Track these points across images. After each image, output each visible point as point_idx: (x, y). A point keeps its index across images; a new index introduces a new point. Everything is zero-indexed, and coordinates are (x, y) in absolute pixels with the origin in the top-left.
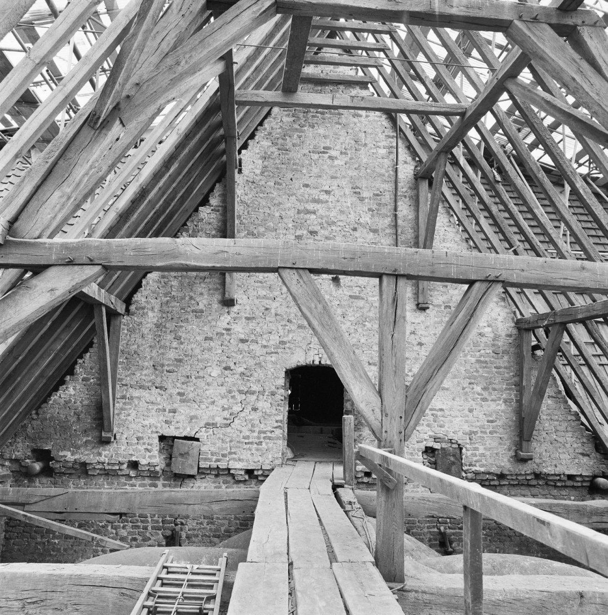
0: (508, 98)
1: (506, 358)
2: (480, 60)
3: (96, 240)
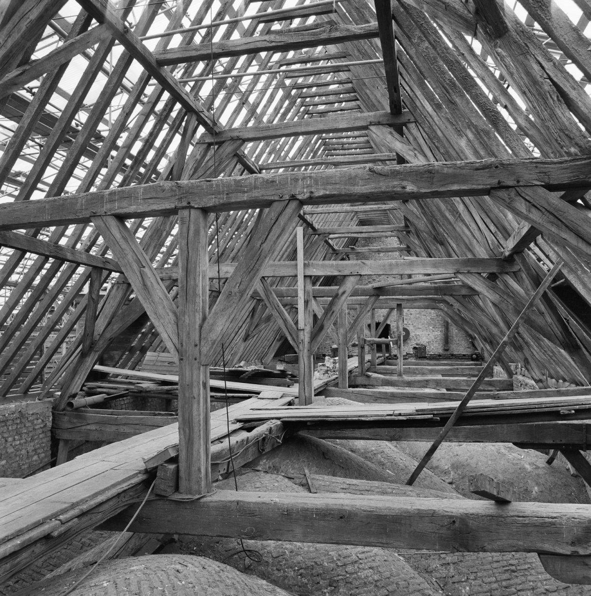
0: (203, 35)
2: (111, 54)
3: (341, 249)
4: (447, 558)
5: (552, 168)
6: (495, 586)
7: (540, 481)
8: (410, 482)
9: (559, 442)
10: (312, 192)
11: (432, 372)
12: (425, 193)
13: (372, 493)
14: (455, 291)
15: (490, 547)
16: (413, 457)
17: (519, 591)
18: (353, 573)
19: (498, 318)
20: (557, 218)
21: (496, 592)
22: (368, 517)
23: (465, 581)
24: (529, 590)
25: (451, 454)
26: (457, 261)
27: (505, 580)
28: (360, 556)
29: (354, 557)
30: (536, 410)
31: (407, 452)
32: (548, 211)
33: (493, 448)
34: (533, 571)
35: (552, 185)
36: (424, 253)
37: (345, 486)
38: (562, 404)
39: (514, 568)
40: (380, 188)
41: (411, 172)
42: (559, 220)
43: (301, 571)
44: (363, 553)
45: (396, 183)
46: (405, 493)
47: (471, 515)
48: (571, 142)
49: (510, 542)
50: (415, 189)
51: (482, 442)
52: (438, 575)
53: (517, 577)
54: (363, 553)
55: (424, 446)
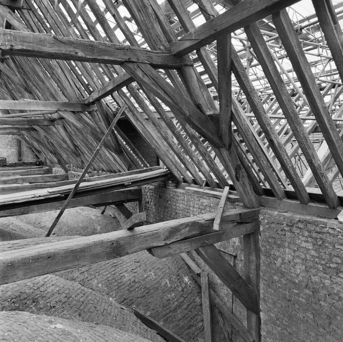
1: (15, 140)
4: (83, 269)
5: (154, 55)
6: (109, 275)
7: (100, 223)
8: (48, 235)
9: (115, 201)
10: (12, 46)
11: (14, 174)
12: (89, 58)
13: (30, 245)
14: (40, 123)
15: (130, 252)
16: (29, 224)
17: (120, 274)
18: (44, 291)
19: (67, 139)
20: (156, 82)
21: (110, 278)
22: (65, 253)
23: (94, 278)
24: (124, 272)
25: (51, 218)
26: (58, 104)
27: (113, 271)
28: (45, 280)
29: (42, 282)
30: (114, 185)
31: (24, 221)
32: (152, 78)
33: (74, 211)
34: (125, 263)
35: (153, 64)
36: (9, 97)
37: (10, 246)
38: (125, 180)
39: (116, 264)
40: (62, 51)
41: (80, 44)
42: (157, 84)
43: (12, 300)
44: (45, 278)
45: (71, 49)
46: (50, 241)
47: (121, 238)
48: (161, 43)
49: (139, 246)
50: (84, 55)
51: (77, 207)
52: (79, 279)
53: (118, 268)
54: (45, 278)
55: (55, 213)
